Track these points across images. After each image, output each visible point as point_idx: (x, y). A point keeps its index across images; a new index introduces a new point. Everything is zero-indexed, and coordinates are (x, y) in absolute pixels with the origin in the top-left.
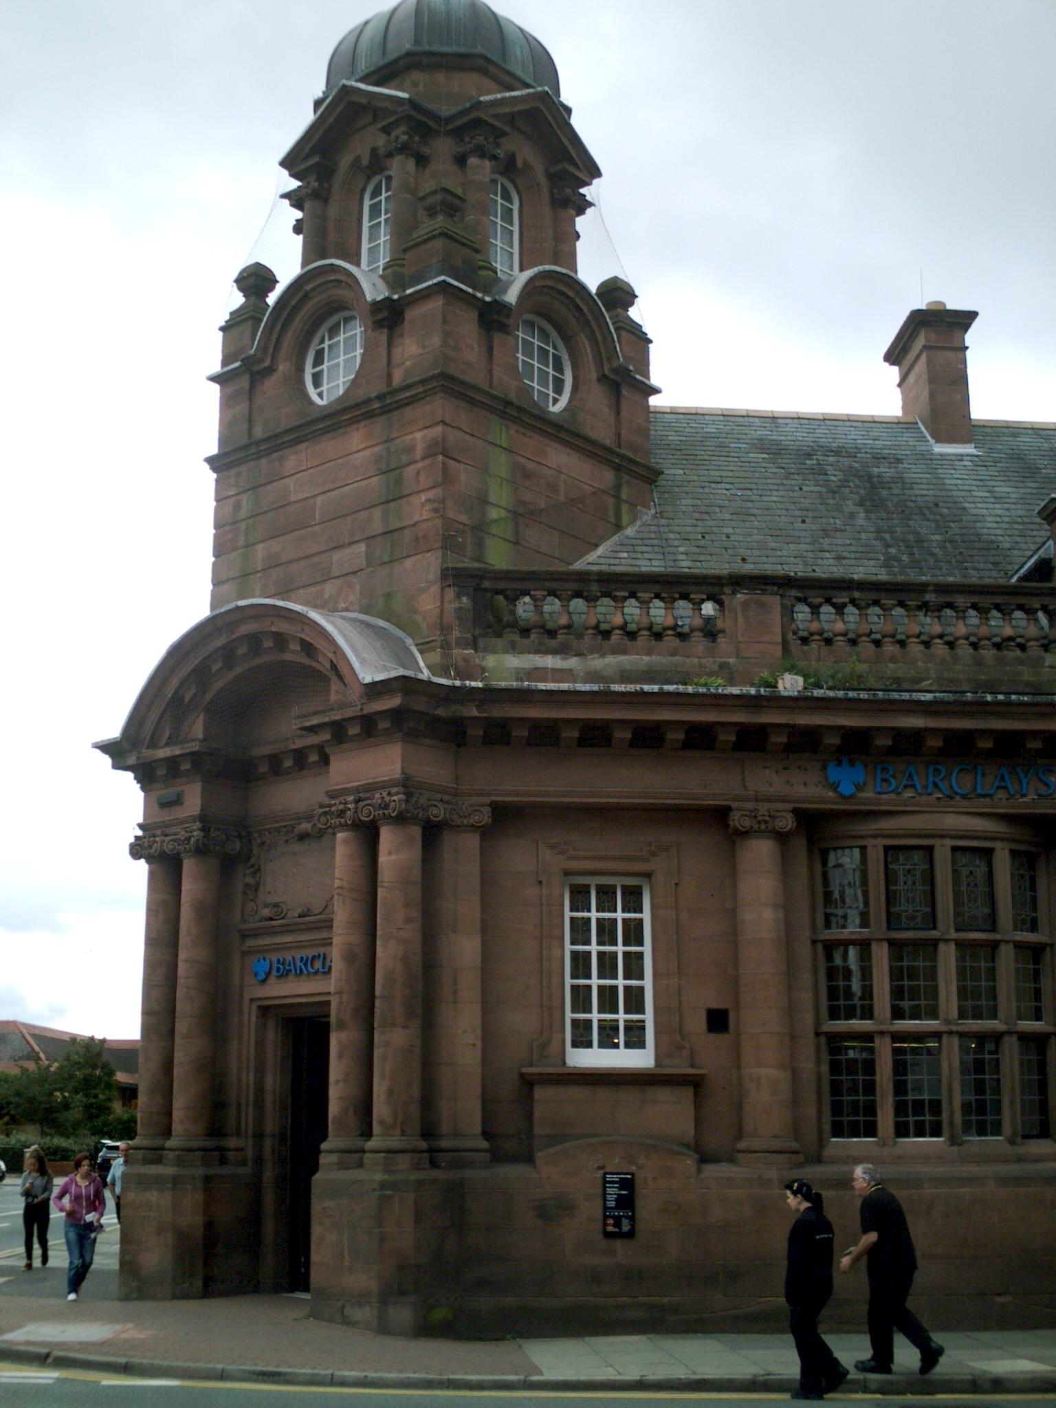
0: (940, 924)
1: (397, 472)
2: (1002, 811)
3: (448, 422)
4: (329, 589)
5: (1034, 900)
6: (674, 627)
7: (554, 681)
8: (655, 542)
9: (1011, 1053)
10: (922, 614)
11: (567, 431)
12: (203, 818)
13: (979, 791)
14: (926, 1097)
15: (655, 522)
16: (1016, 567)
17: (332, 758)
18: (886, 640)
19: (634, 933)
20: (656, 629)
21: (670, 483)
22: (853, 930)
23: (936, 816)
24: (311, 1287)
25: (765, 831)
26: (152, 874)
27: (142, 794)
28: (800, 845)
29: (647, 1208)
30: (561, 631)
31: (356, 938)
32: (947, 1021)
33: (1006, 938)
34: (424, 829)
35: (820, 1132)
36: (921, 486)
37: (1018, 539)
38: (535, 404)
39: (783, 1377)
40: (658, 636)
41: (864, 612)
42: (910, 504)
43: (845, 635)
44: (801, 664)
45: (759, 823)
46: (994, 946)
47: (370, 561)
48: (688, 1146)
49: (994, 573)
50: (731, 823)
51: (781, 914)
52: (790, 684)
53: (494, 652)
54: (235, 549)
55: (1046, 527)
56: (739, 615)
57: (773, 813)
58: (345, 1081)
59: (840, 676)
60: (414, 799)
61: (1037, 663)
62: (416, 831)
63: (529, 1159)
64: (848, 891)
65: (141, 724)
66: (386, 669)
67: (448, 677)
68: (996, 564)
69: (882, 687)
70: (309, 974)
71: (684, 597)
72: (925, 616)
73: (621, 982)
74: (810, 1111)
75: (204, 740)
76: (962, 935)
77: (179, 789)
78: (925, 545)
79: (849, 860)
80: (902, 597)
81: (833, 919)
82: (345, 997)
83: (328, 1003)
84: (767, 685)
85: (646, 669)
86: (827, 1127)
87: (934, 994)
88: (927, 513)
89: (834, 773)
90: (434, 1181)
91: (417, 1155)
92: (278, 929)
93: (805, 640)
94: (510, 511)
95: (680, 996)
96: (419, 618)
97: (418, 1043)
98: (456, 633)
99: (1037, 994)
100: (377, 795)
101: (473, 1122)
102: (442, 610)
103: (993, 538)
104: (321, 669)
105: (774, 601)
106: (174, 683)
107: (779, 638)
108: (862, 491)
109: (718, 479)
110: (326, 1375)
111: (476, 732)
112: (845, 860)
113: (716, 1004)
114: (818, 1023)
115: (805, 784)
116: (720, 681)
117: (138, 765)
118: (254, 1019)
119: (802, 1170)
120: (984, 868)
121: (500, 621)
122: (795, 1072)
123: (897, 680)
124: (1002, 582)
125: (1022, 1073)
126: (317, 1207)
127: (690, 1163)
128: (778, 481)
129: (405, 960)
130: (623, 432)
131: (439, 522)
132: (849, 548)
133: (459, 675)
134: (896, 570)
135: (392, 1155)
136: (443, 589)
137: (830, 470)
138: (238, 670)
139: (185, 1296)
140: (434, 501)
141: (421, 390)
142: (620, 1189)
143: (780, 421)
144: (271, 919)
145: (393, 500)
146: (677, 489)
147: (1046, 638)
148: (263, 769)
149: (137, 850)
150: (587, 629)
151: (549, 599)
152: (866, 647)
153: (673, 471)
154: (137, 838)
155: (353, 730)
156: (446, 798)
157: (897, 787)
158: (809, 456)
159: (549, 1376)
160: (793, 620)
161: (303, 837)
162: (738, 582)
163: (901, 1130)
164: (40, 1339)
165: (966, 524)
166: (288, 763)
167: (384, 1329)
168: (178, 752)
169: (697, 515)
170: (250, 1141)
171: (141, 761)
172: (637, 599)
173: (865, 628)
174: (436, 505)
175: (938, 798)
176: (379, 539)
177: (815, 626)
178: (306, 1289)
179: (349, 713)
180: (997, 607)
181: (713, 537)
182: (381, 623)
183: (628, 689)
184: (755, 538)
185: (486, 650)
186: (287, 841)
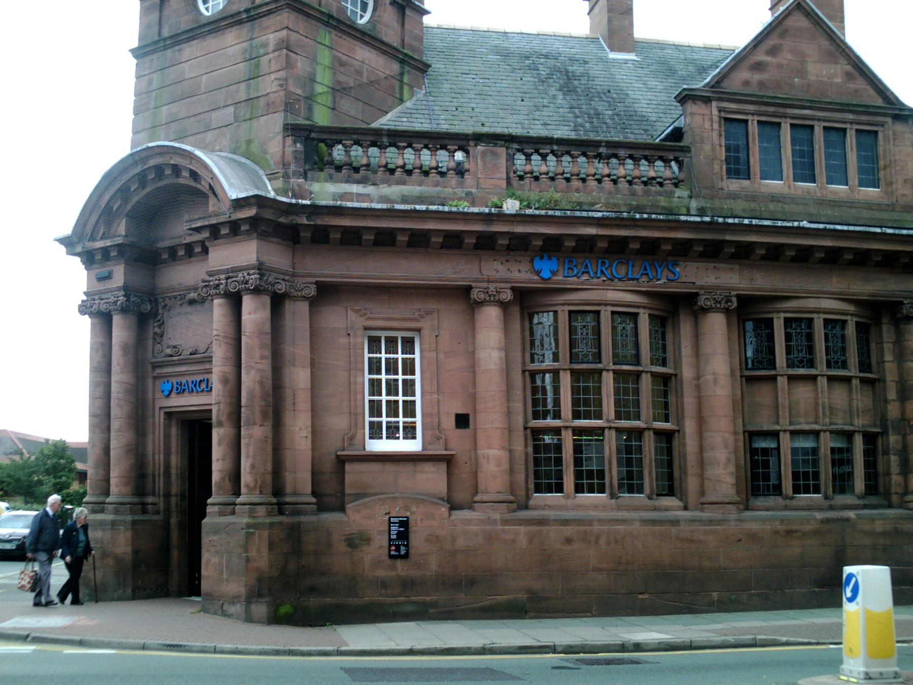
0: (604, 359)
1: (256, 60)
2: (644, 289)
3: (290, 27)
4: (210, 136)
5: (664, 346)
6: (437, 168)
7: (358, 201)
8: (426, 112)
9: (649, 443)
10: (597, 161)
11: (369, 36)
12: (126, 288)
13: (630, 276)
14: (595, 468)
15: (426, 98)
16: (659, 133)
17: (210, 249)
18: (574, 177)
19: (409, 368)
20: (425, 168)
21: (436, 73)
22: (548, 363)
23: (601, 291)
24: (202, 593)
25: (493, 302)
26: (93, 324)
27: (85, 272)
28: (516, 310)
29: (417, 540)
30: (363, 168)
31: (229, 369)
32: (608, 421)
33: (646, 370)
34: (272, 299)
35: (527, 489)
36: (600, 79)
37: (661, 115)
38: (349, 19)
39: (502, 645)
40: (426, 173)
41: (560, 159)
42: (593, 90)
43: (547, 174)
44: (519, 193)
45: (490, 296)
46: (637, 375)
47: (236, 118)
48: (442, 499)
49: (645, 137)
50: (472, 296)
51: (503, 355)
52: (511, 206)
53: (318, 181)
54: (148, 110)
55: (681, 108)
56: (479, 160)
57: (498, 290)
58: (223, 460)
59: (543, 200)
60: (265, 278)
61: (670, 194)
62: (267, 299)
63: (342, 509)
64: (546, 340)
65: (85, 225)
66: (247, 190)
67: (288, 197)
68: (646, 130)
69: (570, 208)
70: (197, 392)
71: (443, 147)
72: (599, 162)
73: (400, 398)
74: (521, 477)
75: (126, 236)
76: (618, 367)
77: (110, 268)
78: (601, 116)
79: (547, 319)
80: (585, 149)
81: (536, 357)
82: (222, 407)
83: (211, 410)
84: (497, 206)
85: (418, 195)
86: (532, 486)
87: (599, 403)
88: (603, 96)
89: (538, 264)
90: (281, 523)
91: (271, 507)
92: (177, 362)
93: (521, 178)
94: (329, 87)
95: (438, 406)
96: (268, 157)
97: (270, 435)
98: (293, 167)
99: (666, 406)
100: (240, 275)
101: (307, 487)
102: (284, 152)
103: (645, 114)
104: (202, 189)
105: (502, 151)
106: (107, 197)
107: (504, 176)
108: (561, 82)
109: (468, 72)
110: (211, 647)
111: (306, 235)
112: (544, 320)
113: (460, 411)
114: (526, 421)
115: (519, 271)
116: (466, 204)
117: (83, 252)
118: (162, 420)
119: (516, 514)
120: (632, 325)
121: (322, 160)
122: (511, 452)
123: (580, 204)
124: (651, 141)
125: (656, 454)
126: (205, 540)
127: (444, 510)
128: (506, 74)
129: (261, 383)
130: (406, 38)
131: (282, 93)
132: (551, 118)
133: (295, 196)
134: (582, 133)
135: (254, 507)
136: (284, 137)
137: (541, 67)
138: (148, 190)
140: (280, 79)
141: (274, 6)
142: (400, 527)
143: (509, 35)
144: (171, 356)
145: (253, 78)
146: (440, 78)
147: (677, 178)
148: (165, 256)
149: (84, 309)
150: (380, 167)
151: (355, 147)
152: (562, 183)
153: (437, 65)
154: (83, 301)
155: (224, 231)
156: (287, 278)
157: (578, 273)
158: (528, 58)
159: (352, 647)
160: (514, 164)
161: (192, 302)
162: (479, 138)
163: (579, 489)
164: (23, 626)
165: (628, 105)
166: (181, 253)
167: (249, 619)
168: (109, 244)
169: (453, 95)
170: (162, 499)
171: (85, 250)
172: (413, 148)
173: (560, 170)
174: (281, 82)
175: (604, 281)
176: (244, 104)
177: (528, 168)
178: (199, 595)
179: (222, 219)
180: (646, 158)
181: (464, 109)
182: (243, 160)
183: (406, 208)
184: (491, 110)
185: (313, 180)
186: (181, 305)
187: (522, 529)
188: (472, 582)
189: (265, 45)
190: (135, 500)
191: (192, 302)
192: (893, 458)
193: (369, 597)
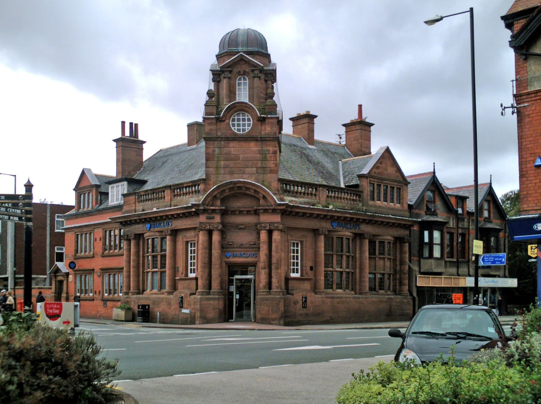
96: (272, 187)
139: (121, 394)
187: (329, 300)
188: (319, 314)
189: (269, 151)
190: (220, 291)
191: (241, 228)
192: (398, 281)
193: (299, 318)
